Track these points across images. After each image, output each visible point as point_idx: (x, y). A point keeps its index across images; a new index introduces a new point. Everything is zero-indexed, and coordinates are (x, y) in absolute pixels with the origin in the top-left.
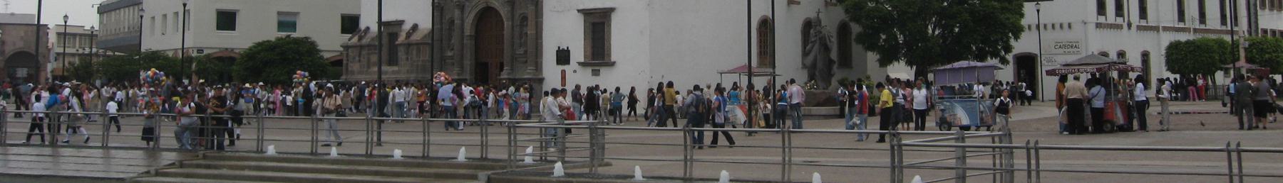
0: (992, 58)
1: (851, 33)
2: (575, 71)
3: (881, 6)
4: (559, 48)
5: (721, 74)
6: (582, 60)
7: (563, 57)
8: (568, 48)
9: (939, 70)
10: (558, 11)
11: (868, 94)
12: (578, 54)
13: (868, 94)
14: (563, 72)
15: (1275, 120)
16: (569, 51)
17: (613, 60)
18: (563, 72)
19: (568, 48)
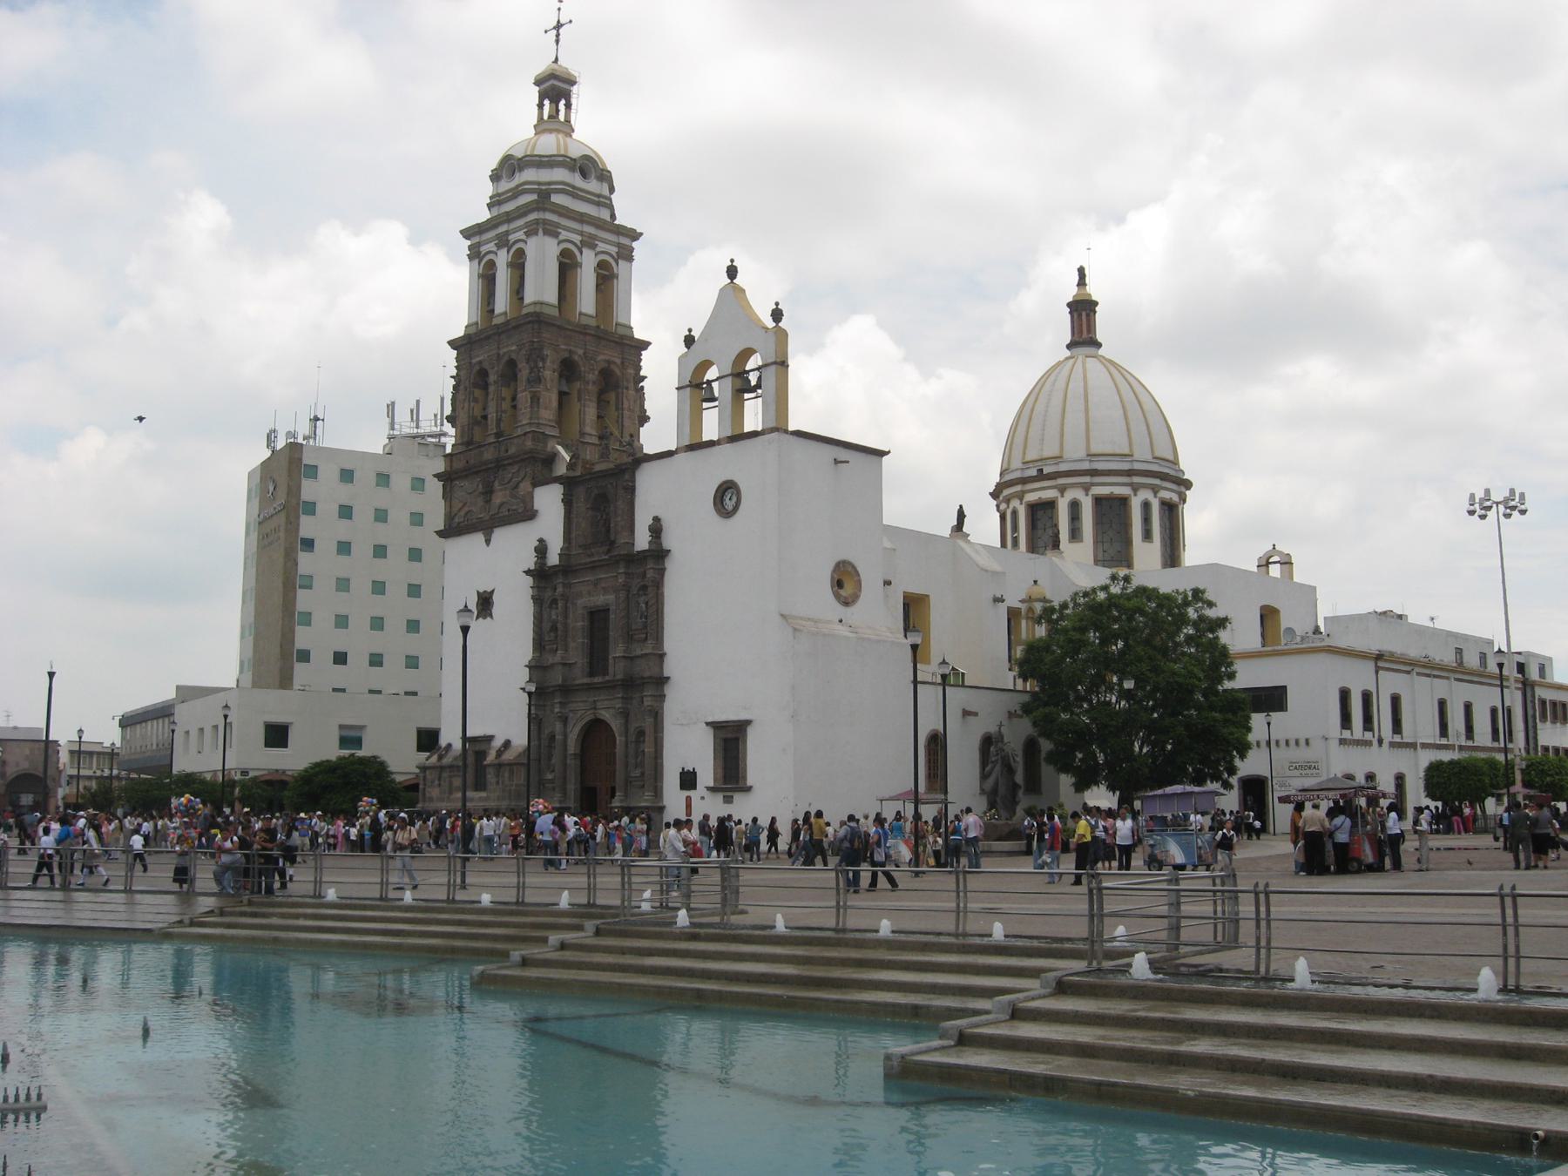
2: (703, 798)
8: (694, 769)
10: (682, 725)
12: (706, 777)
16: (696, 773)
19: (694, 769)
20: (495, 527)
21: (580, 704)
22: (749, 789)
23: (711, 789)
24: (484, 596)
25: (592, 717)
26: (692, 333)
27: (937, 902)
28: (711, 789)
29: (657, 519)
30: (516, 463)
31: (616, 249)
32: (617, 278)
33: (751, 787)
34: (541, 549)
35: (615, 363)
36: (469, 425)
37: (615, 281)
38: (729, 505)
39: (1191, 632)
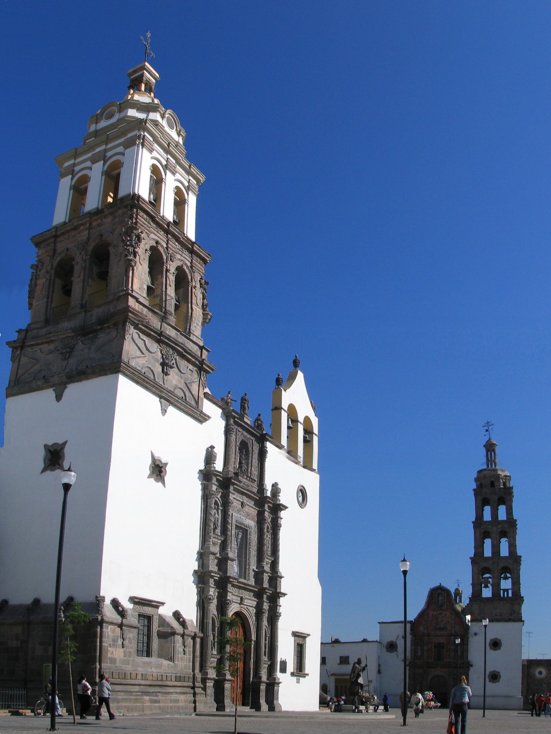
12: (291, 667)
19: (285, 660)
33: (307, 675)
34: (210, 457)
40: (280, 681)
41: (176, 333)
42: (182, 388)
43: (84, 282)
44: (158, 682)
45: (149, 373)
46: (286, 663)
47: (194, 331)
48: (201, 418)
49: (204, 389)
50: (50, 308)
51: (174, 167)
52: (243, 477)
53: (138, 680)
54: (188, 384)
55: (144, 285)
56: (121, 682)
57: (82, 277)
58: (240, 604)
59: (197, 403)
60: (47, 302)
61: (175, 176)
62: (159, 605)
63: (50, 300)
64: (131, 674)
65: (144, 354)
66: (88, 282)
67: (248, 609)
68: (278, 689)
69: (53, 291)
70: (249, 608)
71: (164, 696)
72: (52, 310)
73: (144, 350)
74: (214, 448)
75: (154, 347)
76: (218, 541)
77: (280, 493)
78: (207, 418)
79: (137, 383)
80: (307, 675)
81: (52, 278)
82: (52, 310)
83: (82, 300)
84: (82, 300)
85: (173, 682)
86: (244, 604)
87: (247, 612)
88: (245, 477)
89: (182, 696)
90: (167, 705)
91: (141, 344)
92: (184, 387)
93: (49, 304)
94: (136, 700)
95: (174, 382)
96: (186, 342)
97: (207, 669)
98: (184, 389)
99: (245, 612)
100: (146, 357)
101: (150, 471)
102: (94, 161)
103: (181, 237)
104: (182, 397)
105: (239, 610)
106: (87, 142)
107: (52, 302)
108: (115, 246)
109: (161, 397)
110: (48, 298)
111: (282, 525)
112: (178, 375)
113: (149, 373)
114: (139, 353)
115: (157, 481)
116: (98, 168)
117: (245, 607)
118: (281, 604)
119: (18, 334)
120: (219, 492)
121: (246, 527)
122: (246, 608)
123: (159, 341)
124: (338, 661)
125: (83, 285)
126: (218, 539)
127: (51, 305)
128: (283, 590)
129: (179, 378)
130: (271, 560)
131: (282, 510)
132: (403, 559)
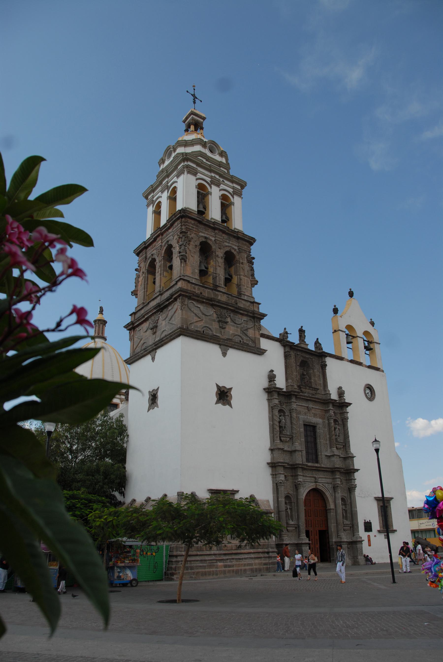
0: (167, 542)
1: (34, 183)
2: (375, 536)
3: (184, 508)
4: (365, 520)
5: (337, 546)
6: (379, 529)
7: (368, 527)
8: (370, 521)
9: (291, 513)
10: (361, 497)
11: (32, 197)
12: (376, 525)
13: (32, 197)
14: (369, 536)
15: (310, 510)
16: (371, 523)
17: (394, 528)
18: (369, 536)
19: (370, 521)
20: (231, 347)
21: (308, 478)
22: (396, 531)
23: (379, 532)
24: (222, 390)
25: (314, 487)
26: (372, 320)
27: (166, 551)
28: (379, 532)
29: (340, 388)
30: (247, 315)
31: (232, 190)
32: (234, 205)
33: (396, 531)
34: (272, 377)
35: (211, 240)
36: (216, 274)
37: (232, 206)
38: (368, 391)
39: (332, 424)
40: (363, 539)
41: (227, 297)
42: (240, 334)
43: (161, 275)
44: (233, 551)
45: (208, 331)
46: (370, 523)
47: (245, 292)
48: (261, 352)
49: (259, 332)
50: (146, 296)
51: (218, 181)
52: (305, 389)
53: (213, 550)
54: (244, 331)
55: (196, 270)
56: (197, 554)
57: (159, 272)
58: (316, 482)
59: (254, 342)
60: (144, 291)
61: (219, 188)
62: (235, 492)
63: (146, 290)
64: (435, 537)
65: (201, 318)
66: (163, 275)
67: (324, 485)
68: (362, 546)
69: (147, 284)
70: (324, 484)
71: (238, 562)
72: (147, 296)
73: (200, 315)
74: (273, 371)
75: (211, 311)
76: (287, 439)
77: (344, 394)
78: (264, 351)
79: (198, 339)
80: (396, 531)
81: (146, 275)
82: (147, 296)
83: (160, 287)
84: (160, 287)
85: (248, 550)
86: (318, 482)
87: (323, 488)
88: (308, 388)
89: (257, 560)
90: (241, 568)
91: (196, 311)
92: (241, 333)
93: (146, 293)
94: (210, 567)
95: (231, 332)
96: (238, 301)
97: (284, 537)
98: (241, 335)
99: (320, 488)
100: (202, 320)
101: (217, 397)
102: (162, 192)
103: (226, 230)
104: (240, 341)
105: (315, 487)
106: (200, 158)
107: (147, 291)
108: (174, 248)
109: (220, 345)
110: (144, 289)
111: (349, 418)
112: (234, 326)
113: (208, 331)
114: (196, 319)
115: (224, 404)
116: (165, 195)
117: (321, 484)
118: (355, 478)
119: (130, 316)
120: (283, 403)
121: (315, 424)
122: (322, 485)
123: (213, 305)
124: (367, 520)
125: (161, 278)
126: (286, 437)
127: (146, 293)
128: (356, 467)
129: (235, 328)
130: (342, 445)
131: (347, 407)
132: (374, 440)
